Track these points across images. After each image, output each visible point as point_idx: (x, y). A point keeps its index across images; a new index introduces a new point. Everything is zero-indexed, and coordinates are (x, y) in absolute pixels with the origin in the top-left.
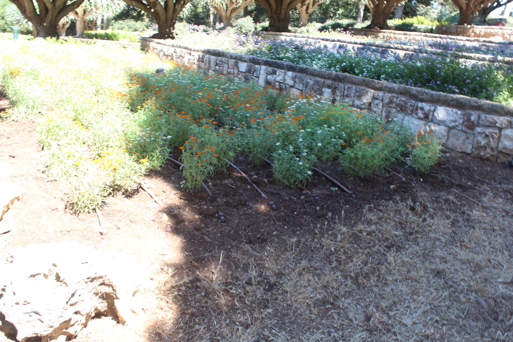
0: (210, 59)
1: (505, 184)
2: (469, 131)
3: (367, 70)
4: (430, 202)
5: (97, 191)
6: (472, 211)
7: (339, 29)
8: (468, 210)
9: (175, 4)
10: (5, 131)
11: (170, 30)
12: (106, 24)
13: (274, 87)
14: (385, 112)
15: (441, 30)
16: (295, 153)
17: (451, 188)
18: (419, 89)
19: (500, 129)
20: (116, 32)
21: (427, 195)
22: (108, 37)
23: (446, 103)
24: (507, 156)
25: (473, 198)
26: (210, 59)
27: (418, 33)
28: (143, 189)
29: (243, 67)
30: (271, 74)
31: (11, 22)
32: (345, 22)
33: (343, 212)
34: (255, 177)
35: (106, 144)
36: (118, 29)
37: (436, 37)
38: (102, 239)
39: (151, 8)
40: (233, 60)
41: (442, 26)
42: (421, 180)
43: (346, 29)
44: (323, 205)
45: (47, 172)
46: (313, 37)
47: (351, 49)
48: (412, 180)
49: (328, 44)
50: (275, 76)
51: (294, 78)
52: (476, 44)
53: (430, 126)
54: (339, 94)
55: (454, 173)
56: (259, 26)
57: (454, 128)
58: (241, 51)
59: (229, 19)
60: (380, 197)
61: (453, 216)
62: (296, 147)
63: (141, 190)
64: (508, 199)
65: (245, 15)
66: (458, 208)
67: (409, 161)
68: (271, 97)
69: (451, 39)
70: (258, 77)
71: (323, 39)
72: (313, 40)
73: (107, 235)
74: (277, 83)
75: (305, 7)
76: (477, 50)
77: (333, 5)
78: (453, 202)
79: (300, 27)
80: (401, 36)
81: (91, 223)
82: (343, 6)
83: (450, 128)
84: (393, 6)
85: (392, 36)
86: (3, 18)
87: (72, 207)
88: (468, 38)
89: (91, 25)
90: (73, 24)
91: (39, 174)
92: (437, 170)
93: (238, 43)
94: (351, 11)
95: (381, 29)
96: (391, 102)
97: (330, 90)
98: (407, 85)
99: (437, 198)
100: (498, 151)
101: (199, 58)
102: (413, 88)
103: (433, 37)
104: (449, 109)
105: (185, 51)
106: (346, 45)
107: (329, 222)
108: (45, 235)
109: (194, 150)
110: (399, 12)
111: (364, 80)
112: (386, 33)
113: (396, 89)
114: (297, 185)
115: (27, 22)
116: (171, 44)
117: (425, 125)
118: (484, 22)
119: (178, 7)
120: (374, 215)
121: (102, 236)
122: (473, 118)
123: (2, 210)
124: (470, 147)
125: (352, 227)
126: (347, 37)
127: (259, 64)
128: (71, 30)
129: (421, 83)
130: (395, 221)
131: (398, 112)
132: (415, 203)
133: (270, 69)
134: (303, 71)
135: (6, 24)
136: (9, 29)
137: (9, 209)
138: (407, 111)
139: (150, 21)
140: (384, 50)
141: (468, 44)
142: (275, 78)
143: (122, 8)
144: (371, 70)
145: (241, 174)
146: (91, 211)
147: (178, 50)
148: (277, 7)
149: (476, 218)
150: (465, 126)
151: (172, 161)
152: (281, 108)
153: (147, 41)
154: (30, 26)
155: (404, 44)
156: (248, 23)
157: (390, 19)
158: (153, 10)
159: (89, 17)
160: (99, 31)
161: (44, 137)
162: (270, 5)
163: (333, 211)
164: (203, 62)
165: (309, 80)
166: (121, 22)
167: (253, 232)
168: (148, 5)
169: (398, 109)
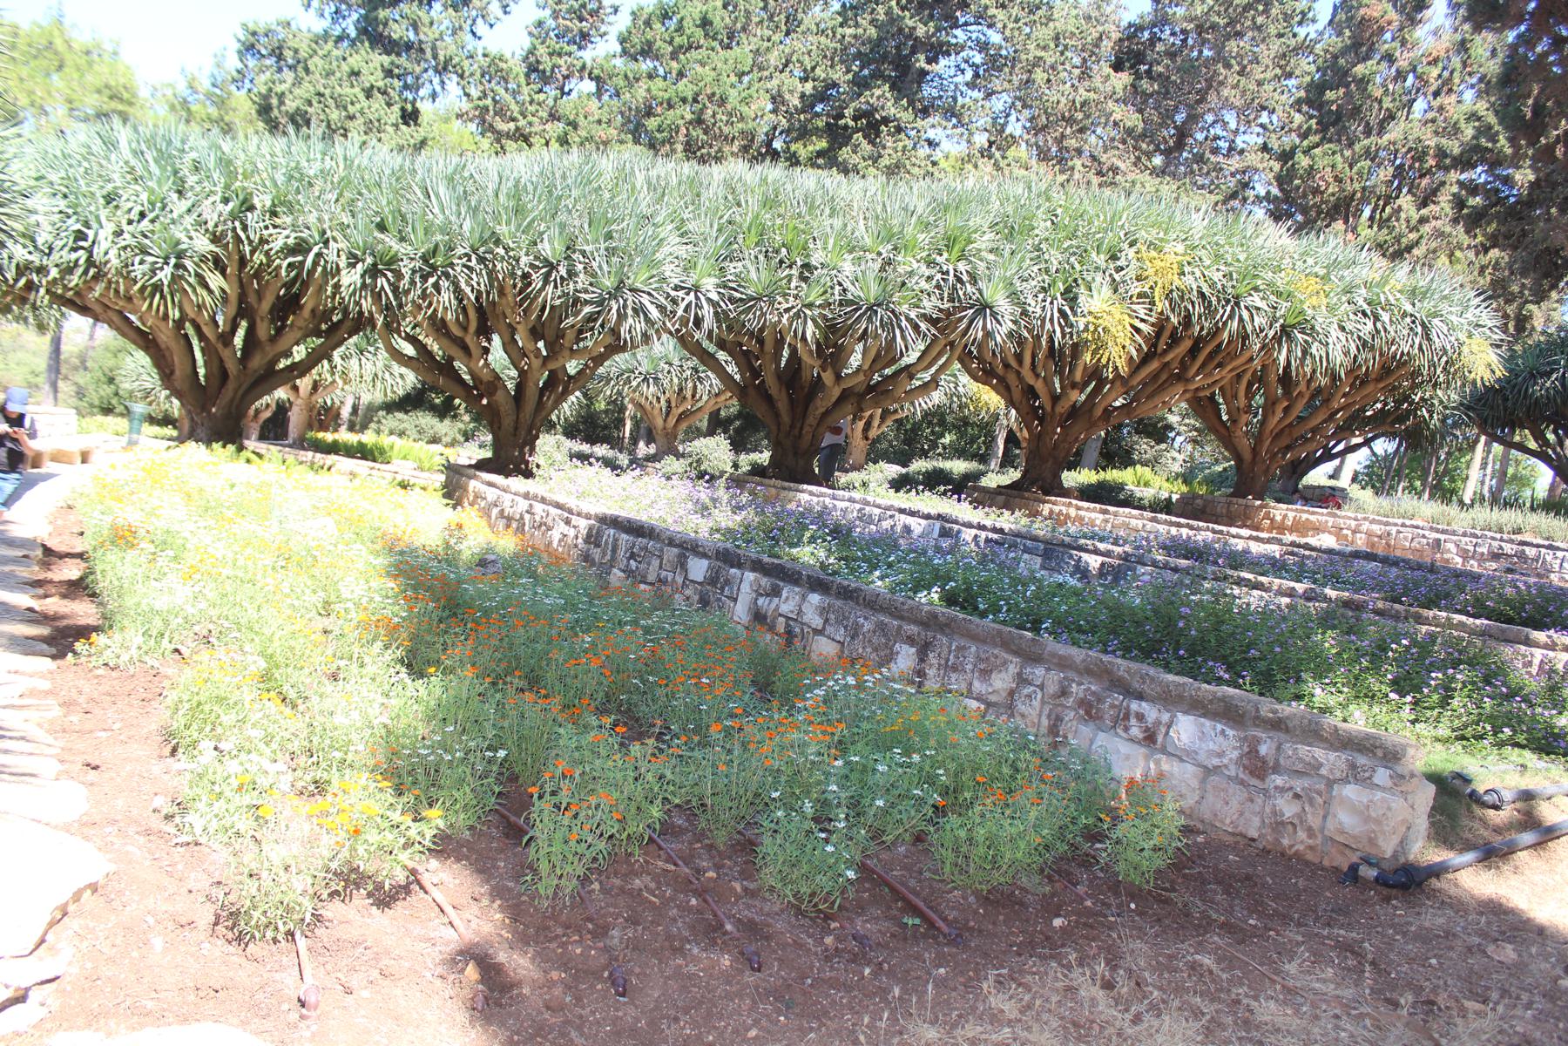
0: (616, 540)
1: (1342, 927)
2: (1254, 781)
3: (1008, 604)
4: (1153, 970)
5: (301, 883)
6: (1256, 998)
7: (942, 488)
8: (1247, 996)
9: (542, 391)
10: (80, 693)
11: (522, 454)
12: (363, 418)
13: (772, 628)
14: (1049, 716)
15: (1189, 508)
16: (816, 820)
17: (1206, 932)
18: (1134, 666)
19: (1330, 783)
20: (386, 440)
21: (1145, 948)
22: (364, 453)
23: (1198, 707)
24: (1347, 851)
25: (1261, 964)
26: (616, 540)
27: (1135, 512)
28: (422, 887)
29: (698, 568)
30: (767, 595)
31: (131, 392)
32: (958, 466)
33: (930, 987)
34: (711, 874)
35: (338, 755)
36: (391, 433)
37: (1179, 525)
38: (302, 1017)
39: (481, 397)
40: (675, 550)
41: (1195, 496)
42: (1133, 906)
43: (960, 487)
44: (880, 964)
45: (178, 819)
46: (879, 501)
47: (969, 539)
48: (1109, 906)
49: (910, 520)
50: (776, 600)
51: (823, 611)
52: (1275, 550)
53: (1157, 763)
54: (934, 661)
55: (1216, 893)
56: (745, 460)
57: (1216, 770)
58: (699, 527)
59: (671, 436)
60: (1029, 947)
61: (1209, 1009)
62: (824, 804)
63: (415, 887)
64: (1349, 970)
65: (711, 433)
66: (1221, 990)
67: (1103, 850)
68: (765, 654)
69: (1214, 532)
70: (735, 600)
71: (902, 511)
72: (877, 511)
73: (316, 1008)
74: (781, 620)
75: (861, 424)
76: (1276, 566)
77: (930, 423)
78: (1211, 972)
79: (847, 471)
80: (1093, 515)
81: (280, 973)
82: (954, 426)
83: (1208, 771)
84: (1077, 439)
85: (1072, 512)
86: (111, 380)
87: (234, 925)
88: (1255, 533)
89: (326, 417)
90: (282, 410)
91: (156, 823)
92: (1173, 882)
93: (690, 505)
94: (973, 440)
95: (1047, 493)
96: (1064, 692)
97: (914, 650)
98: (1106, 652)
99: (1171, 957)
100: (1324, 837)
101: (589, 536)
102: (1119, 661)
103: (1172, 524)
104: (1208, 723)
105: (554, 511)
106: (959, 532)
107: (893, 1012)
108: (154, 995)
109: (564, 798)
110: (1092, 452)
111: (999, 632)
112: (1059, 505)
113: (1078, 660)
114: (815, 905)
115: (167, 397)
116: (522, 490)
117: (1147, 758)
118: (1293, 492)
119: (549, 400)
120: (1011, 998)
121: (304, 1011)
122: (1263, 750)
123: (48, 919)
124: (1256, 821)
125: (954, 1026)
126: (962, 510)
127: (739, 566)
128: (275, 429)
129: (1141, 649)
130: (1062, 1018)
131: (1082, 720)
132: (1114, 968)
133: (765, 582)
134: (847, 594)
135: (117, 394)
136: (120, 409)
137: (65, 914)
138: (1101, 718)
139: (473, 420)
140: (1054, 551)
141: (1256, 548)
142: (778, 606)
143: (409, 386)
144: (1017, 604)
145: (675, 864)
146: (280, 937)
147: (539, 508)
148: (793, 419)
149: (1267, 1018)
150: (1245, 767)
151: (503, 816)
152: (786, 692)
153: (462, 475)
154: (176, 407)
155: (1102, 540)
156: (717, 451)
157: (1069, 470)
158: (485, 402)
159: (325, 398)
160: (344, 436)
161: (179, 722)
162: (777, 415)
163: (904, 981)
164: (598, 545)
165: (861, 620)
166: (400, 415)
167: (699, 1028)
168: (475, 387)
169: (1082, 712)
